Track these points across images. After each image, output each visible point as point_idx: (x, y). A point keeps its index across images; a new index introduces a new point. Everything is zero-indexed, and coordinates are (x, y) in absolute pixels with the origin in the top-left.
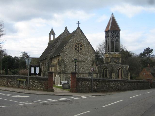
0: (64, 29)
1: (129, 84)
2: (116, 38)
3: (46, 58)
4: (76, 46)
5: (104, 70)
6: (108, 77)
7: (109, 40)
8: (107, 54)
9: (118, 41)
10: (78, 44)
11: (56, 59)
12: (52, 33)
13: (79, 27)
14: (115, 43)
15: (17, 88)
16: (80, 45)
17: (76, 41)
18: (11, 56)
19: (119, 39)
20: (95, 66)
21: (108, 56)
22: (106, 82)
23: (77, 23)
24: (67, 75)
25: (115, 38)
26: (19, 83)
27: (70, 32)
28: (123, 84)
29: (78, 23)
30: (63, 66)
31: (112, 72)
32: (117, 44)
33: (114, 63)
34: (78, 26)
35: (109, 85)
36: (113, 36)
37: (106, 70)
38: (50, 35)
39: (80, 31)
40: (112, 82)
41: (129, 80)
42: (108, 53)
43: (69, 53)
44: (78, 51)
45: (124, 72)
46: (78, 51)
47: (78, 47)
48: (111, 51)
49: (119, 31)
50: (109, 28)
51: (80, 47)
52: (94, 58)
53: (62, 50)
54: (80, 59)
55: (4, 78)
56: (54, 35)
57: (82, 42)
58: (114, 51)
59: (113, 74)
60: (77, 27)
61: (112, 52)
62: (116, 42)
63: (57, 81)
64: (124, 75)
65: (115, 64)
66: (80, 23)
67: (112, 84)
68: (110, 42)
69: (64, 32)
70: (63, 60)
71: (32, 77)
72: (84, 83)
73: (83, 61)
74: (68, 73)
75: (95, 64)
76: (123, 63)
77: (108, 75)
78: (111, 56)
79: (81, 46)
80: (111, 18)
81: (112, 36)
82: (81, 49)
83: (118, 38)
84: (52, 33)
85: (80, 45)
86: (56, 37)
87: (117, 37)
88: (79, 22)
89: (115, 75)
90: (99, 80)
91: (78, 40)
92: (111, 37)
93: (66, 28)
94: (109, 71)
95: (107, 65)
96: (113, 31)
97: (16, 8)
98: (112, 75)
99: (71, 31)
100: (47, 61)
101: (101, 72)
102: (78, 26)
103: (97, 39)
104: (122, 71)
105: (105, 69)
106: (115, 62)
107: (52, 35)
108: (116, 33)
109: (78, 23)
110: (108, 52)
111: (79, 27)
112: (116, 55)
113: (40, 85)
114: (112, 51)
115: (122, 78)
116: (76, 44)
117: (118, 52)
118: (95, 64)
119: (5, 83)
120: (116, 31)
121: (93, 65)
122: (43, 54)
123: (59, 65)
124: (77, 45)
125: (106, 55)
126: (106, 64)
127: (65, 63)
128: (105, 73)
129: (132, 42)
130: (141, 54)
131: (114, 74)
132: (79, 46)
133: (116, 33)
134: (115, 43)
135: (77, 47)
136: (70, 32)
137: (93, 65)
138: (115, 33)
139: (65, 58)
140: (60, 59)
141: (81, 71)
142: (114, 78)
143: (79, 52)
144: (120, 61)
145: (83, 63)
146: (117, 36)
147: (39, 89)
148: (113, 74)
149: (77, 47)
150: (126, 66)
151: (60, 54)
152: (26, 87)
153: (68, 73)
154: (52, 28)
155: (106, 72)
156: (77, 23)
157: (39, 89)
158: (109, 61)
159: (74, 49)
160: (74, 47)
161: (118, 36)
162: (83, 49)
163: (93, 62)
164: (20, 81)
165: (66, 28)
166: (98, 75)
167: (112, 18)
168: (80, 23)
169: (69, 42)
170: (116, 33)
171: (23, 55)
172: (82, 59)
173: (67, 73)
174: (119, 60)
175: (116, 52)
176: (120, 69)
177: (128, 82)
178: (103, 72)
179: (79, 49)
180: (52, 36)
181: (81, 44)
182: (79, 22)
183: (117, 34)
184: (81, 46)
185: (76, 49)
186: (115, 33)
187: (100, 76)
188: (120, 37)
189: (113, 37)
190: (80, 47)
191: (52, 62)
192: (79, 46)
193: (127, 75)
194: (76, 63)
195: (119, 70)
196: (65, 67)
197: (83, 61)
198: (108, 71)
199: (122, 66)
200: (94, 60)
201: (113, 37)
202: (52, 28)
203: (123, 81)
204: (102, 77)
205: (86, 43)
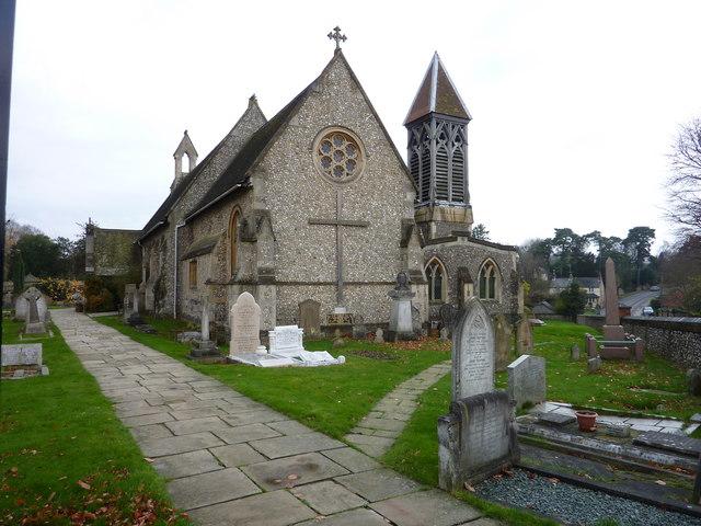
0: (245, 106)
2: (453, 145)
4: (326, 144)
7: (428, 152)
12: (186, 147)
17: (327, 119)
18: (47, 238)
19: (466, 151)
20: (414, 248)
23: (330, 36)
24: (286, 290)
27: (269, 118)
33: (466, 242)
34: (338, 52)
37: (439, 271)
38: (177, 156)
39: (345, 74)
43: (285, 187)
44: (339, 170)
46: (339, 170)
48: (438, 198)
49: (464, 119)
50: (428, 104)
54: (347, 213)
56: (192, 153)
57: (357, 130)
58: (446, 199)
59: (466, 286)
60: (331, 55)
63: (246, 327)
65: (471, 244)
66: (344, 38)
69: (244, 116)
73: (363, 226)
75: (414, 239)
81: (442, 137)
82: (351, 163)
84: (186, 147)
86: (199, 161)
88: (341, 33)
91: (339, 121)
93: (253, 100)
97: (237, 512)
100: (172, 237)
102: (338, 52)
109: (337, 35)
116: (328, 136)
120: (453, 119)
121: (404, 244)
126: (438, 246)
127: (276, 228)
133: (453, 127)
134: (450, 163)
137: (404, 244)
139: (273, 206)
143: (344, 178)
145: (360, 232)
146: (457, 140)
148: (468, 288)
153: (291, 283)
154: (186, 133)
159: (317, 159)
160: (321, 154)
161: (461, 139)
162: (363, 165)
165: (253, 100)
167: (436, 68)
168: (344, 38)
170: (453, 127)
172: (356, 216)
173: (286, 283)
176: (487, 265)
179: (343, 163)
180: (185, 159)
182: (341, 33)
183: (459, 131)
185: (326, 161)
191: (191, 239)
197: (363, 226)
198: (445, 278)
199: (498, 255)
202: (186, 133)
205: (375, 136)
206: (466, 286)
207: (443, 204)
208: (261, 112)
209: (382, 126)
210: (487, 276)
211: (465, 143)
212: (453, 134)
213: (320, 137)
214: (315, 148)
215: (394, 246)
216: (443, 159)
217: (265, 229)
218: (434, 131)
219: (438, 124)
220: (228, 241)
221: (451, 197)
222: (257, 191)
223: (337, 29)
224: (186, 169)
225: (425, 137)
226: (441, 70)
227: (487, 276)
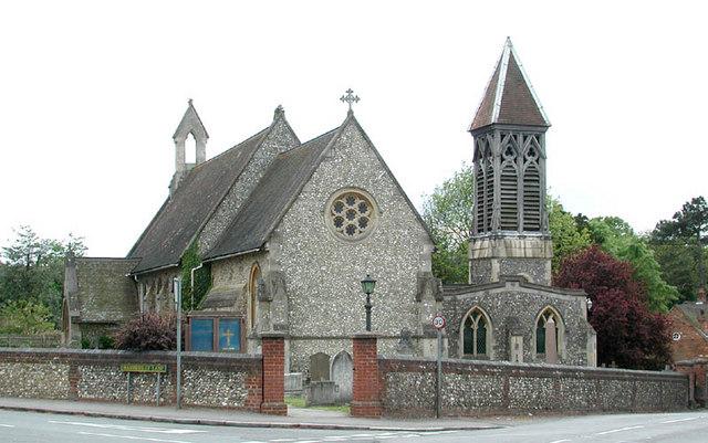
0: (268, 121)
1: (592, 384)
2: (525, 160)
3: (180, 263)
4: (338, 207)
5: (469, 322)
6: (491, 352)
7: (491, 171)
8: (483, 239)
9: (535, 177)
10: (351, 201)
11: (241, 268)
12: (191, 126)
13: (351, 118)
14: (521, 183)
15: (122, 401)
16: (358, 202)
20: (429, 303)
21: (486, 253)
22: (493, 374)
23: (342, 99)
25: (521, 159)
26: (131, 382)
27: (304, 137)
28: (564, 385)
29: (350, 97)
30: (280, 305)
31: (510, 327)
32: (534, 189)
33: (517, 288)
34: (350, 112)
35: (507, 388)
36: (512, 154)
37: (482, 322)
38: (179, 136)
40: (517, 376)
41: (592, 365)
42: (490, 237)
44: (351, 230)
45: (567, 332)
47: (351, 214)
48: (503, 228)
49: (538, 127)
51: (359, 215)
52: (426, 267)
53: (276, 227)
55: (57, 362)
56: (201, 135)
58: (516, 229)
61: (507, 233)
62: (525, 181)
64: (568, 347)
65: (523, 290)
66: (357, 99)
67: (519, 387)
68: (497, 180)
70: (280, 279)
71: (194, 358)
72: (408, 378)
74: (305, 338)
75: (428, 293)
76: (562, 283)
77: (491, 343)
78: (503, 254)
79: (363, 208)
80: (495, 77)
81: (509, 152)
82: (363, 223)
83: (537, 161)
84: (191, 126)
85: (358, 202)
86: (214, 149)
87: (530, 159)
89: (527, 346)
90: (467, 365)
91: (350, 182)
92: (502, 160)
93: (279, 112)
94: (493, 327)
95: (485, 298)
96: (511, 128)
98: (508, 344)
99: (306, 132)
101: (458, 332)
102: (350, 112)
103: (429, 157)
104: (561, 326)
105: (475, 313)
106: (525, 283)
107: (190, 136)
108: (529, 140)
109: (350, 97)
110: (490, 229)
111: (351, 118)
112: (524, 244)
113: (231, 388)
114: (508, 228)
115: (560, 357)
117: (537, 230)
118: (428, 293)
119: (63, 384)
120: (525, 128)
121: (419, 298)
122: (147, 231)
123: (262, 300)
124: (344, 201)
125: (479, 243)
127: (290, 287)
128: (475, 333)
129: (616, 177)
130: (666, 229)
131: (520, 339)
132: (355, 207)
133: (525, 138)
134: (521, 183)
135: (343, 214)
136: (304, 137)
137: (419, 298)
138: (520, 138)
140: (266, 269)
141: (309, 327)
142: (518, 358)
143: (356, 235)
144: (548, 276)
146: (531, 153)
147: (224, 404)
148: (516, 341)
149: (343, 214)
150: (579, 298)
151: (267, 245)
152: (162, 400)
153: (305, 338)
155: (482, 331)
156: (342, 99)
157: (225, 407)
158: (495, 279)
159: (329, 221)
161: (537, 153)
162: (374, 222)
163: (422, 282)
164: (134, 374)
165: (279, 112)
166: (442, 343)
167: (506, 60)
168: (357, 99)
169: (308, 187)
170: (525, 138)
171: (20, 238)
173: (300, 338)
174: (543, 271)
175: (525, 229)
176: (547, 314)
177: (589, 375)
178: (469, 331)
179: (355, 221)
180: (190, 142)
181: (361, 197)
182: (354, 95)
183: (532, 142)
184: (363, 208)
185: (338, 222)
186: (520, 138)
187: (453, 351)
188: (544, 158)
189: (512, 158)
190: (359, 215)
192: (355, 207)
193: (583, 343)
194: (368, 294)
195: (541, 322)
196: (290, 308)
200: (426, 273)
201: (512, 158)
203: (568, 374)
204: (534, 354)
206: (514, 338)
207: (512, 236)
208: (289, 128)
209: (395, 182)
210: (475, 326)
211: (541, 158)
212: (524, 147)
213: (333, 199)
214: (328, 211)
215: (409, 301)
216: (509, 178)
217: (281, 290)
218: (497, 146)
219: (503, 137)
220: (249, 294)
221: (521, 226)
222: (272, 253)
223: (350, 91)
224: (191, 158)
225: (489, 153)
226: (511, 56)
227: (475, 326)
